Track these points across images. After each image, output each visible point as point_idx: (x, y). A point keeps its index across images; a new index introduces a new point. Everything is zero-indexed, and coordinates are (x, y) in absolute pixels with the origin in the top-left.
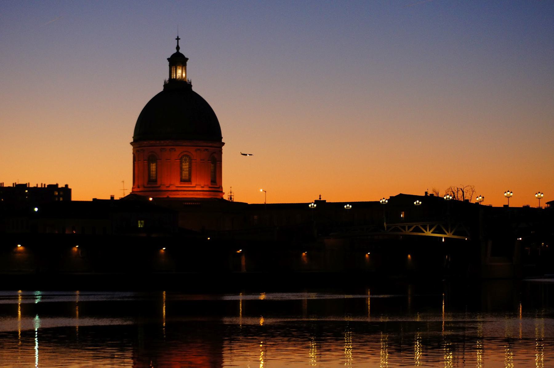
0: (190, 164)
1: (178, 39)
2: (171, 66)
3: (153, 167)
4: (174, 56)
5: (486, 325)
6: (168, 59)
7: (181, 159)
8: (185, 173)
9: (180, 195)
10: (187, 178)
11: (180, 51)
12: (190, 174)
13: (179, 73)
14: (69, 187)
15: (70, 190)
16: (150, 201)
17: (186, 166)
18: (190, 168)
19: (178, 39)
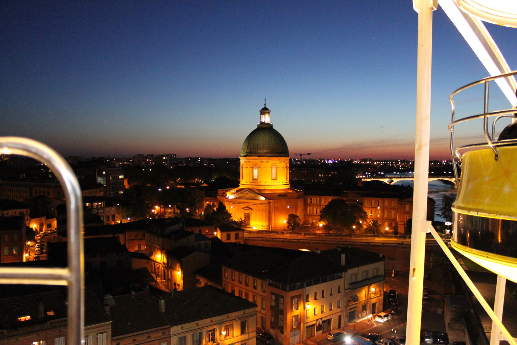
0: (277, 170)
1: (265, 100)
2: (439, 7)
3: (256, 171)
4: (263, 109)
5: (381, 244)
6: (260, 111)
7: (253, 167)
8: (274, 176)
9: (267, 188)
10: (275, 178)
11: (267, 107)
12: (276, 176)
13: (267, 119)
14: (502, 340)
15: (504, 341)
16: (353, 225)
17: (274, 171)
18: (277, 172)
19: (265, 100)
